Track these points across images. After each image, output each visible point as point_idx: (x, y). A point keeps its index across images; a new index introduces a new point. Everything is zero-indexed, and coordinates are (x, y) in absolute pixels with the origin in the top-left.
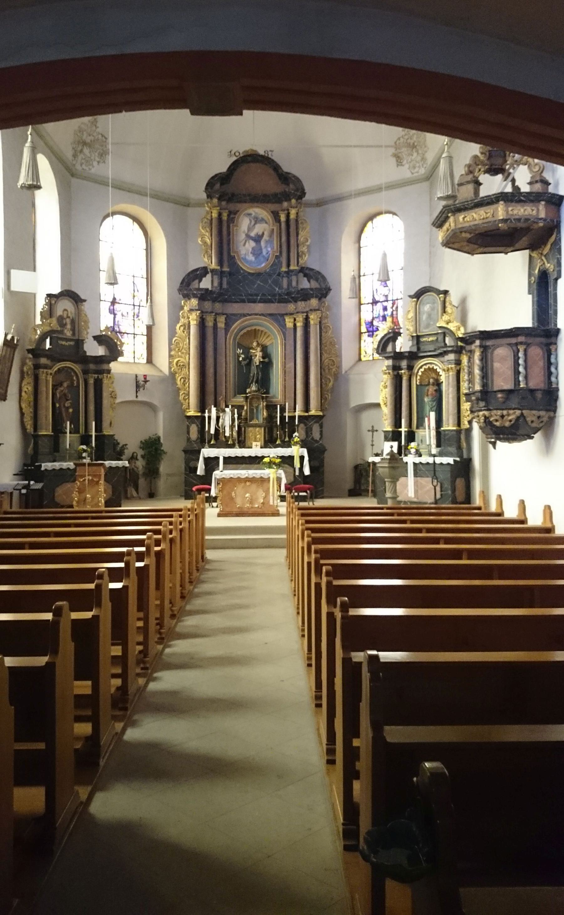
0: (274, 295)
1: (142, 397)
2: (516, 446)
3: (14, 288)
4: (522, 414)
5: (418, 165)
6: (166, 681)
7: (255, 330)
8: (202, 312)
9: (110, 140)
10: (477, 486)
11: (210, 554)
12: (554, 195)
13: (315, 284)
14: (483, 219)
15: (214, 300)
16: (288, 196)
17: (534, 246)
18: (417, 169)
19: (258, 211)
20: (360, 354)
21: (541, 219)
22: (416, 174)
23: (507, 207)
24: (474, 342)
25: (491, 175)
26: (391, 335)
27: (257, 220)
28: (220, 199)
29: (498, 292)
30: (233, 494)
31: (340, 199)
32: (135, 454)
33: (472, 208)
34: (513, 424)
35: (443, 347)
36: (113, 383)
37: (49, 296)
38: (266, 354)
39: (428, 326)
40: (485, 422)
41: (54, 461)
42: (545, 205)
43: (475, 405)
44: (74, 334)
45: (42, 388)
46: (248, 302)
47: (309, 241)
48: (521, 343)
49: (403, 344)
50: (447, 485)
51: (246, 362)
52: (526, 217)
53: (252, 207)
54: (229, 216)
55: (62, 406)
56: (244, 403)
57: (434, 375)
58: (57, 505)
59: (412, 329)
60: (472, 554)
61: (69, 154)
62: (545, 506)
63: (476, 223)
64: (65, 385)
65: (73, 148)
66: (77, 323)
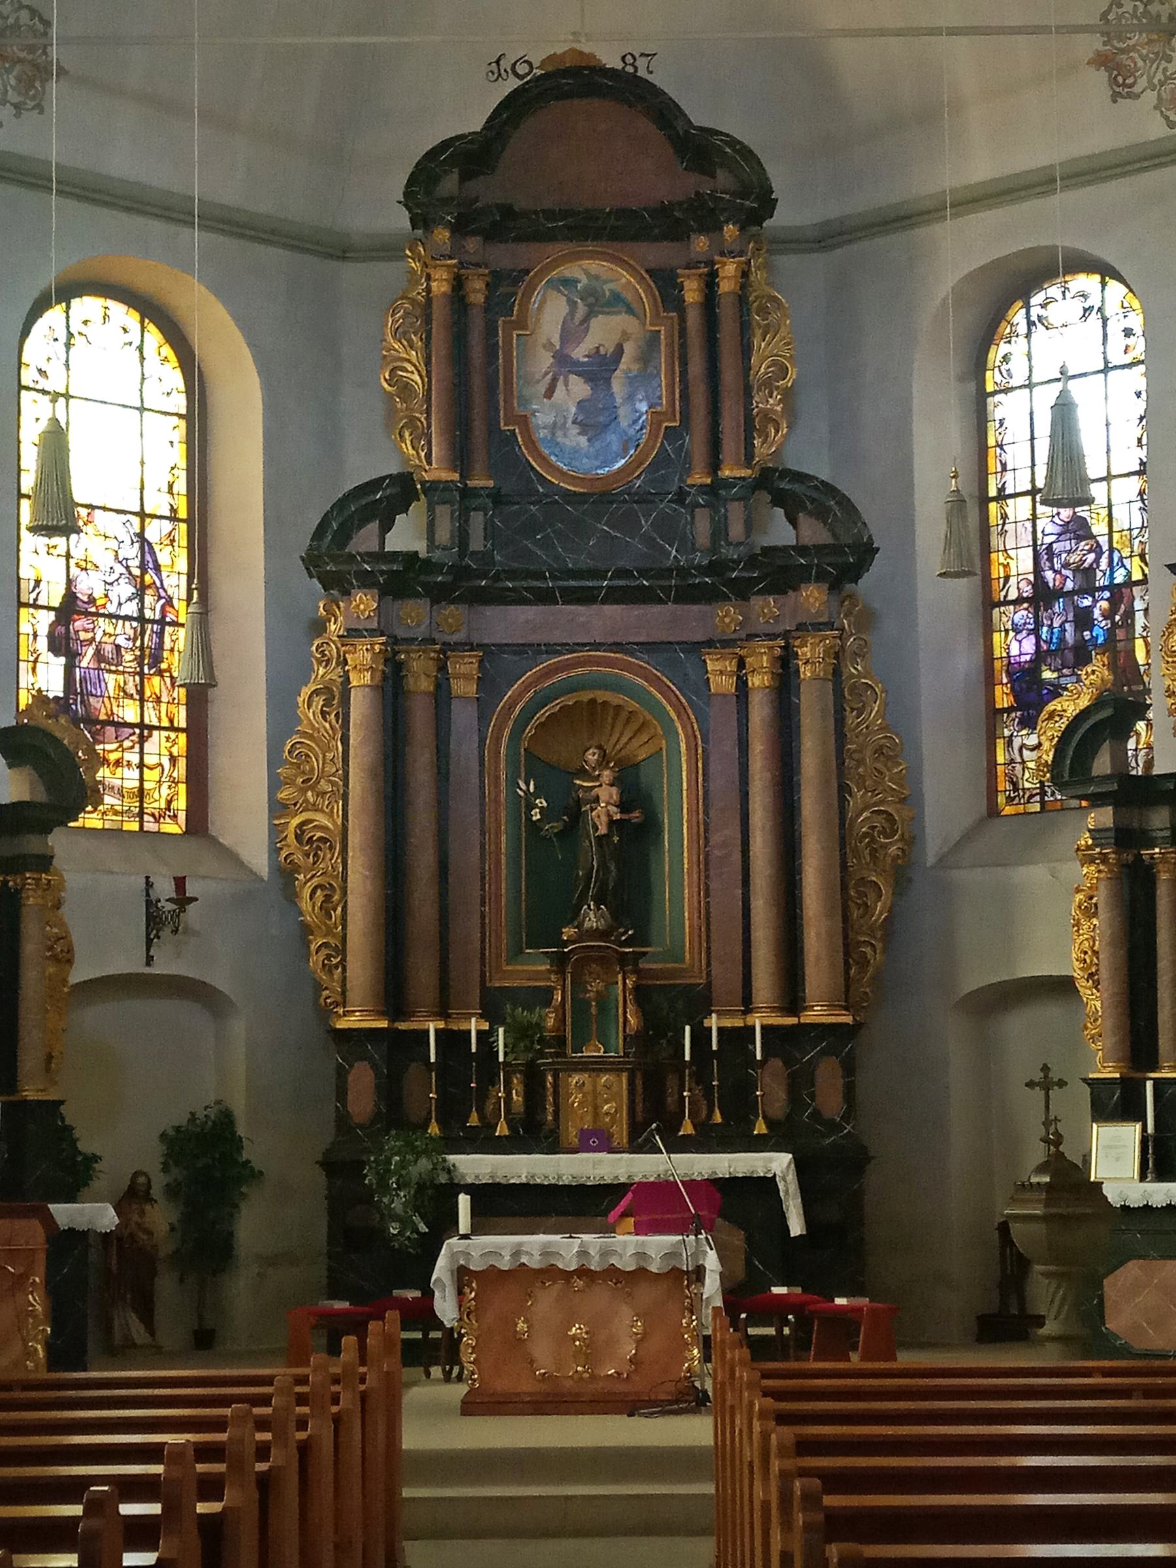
0: (666, 573)
7: (593, 701)
8: (395, 640)
13: (813, 532)
15: (439, 595)
19: (592, 269)
20: (992, 791)
26: (1107, 713)
27: (599, 302)
28: (460, 229)
30: (521, 1326)
31: (902, 219)
32: (142, 1180)
36: (58, 905)
47: (792, 374)
51: (557, 826)
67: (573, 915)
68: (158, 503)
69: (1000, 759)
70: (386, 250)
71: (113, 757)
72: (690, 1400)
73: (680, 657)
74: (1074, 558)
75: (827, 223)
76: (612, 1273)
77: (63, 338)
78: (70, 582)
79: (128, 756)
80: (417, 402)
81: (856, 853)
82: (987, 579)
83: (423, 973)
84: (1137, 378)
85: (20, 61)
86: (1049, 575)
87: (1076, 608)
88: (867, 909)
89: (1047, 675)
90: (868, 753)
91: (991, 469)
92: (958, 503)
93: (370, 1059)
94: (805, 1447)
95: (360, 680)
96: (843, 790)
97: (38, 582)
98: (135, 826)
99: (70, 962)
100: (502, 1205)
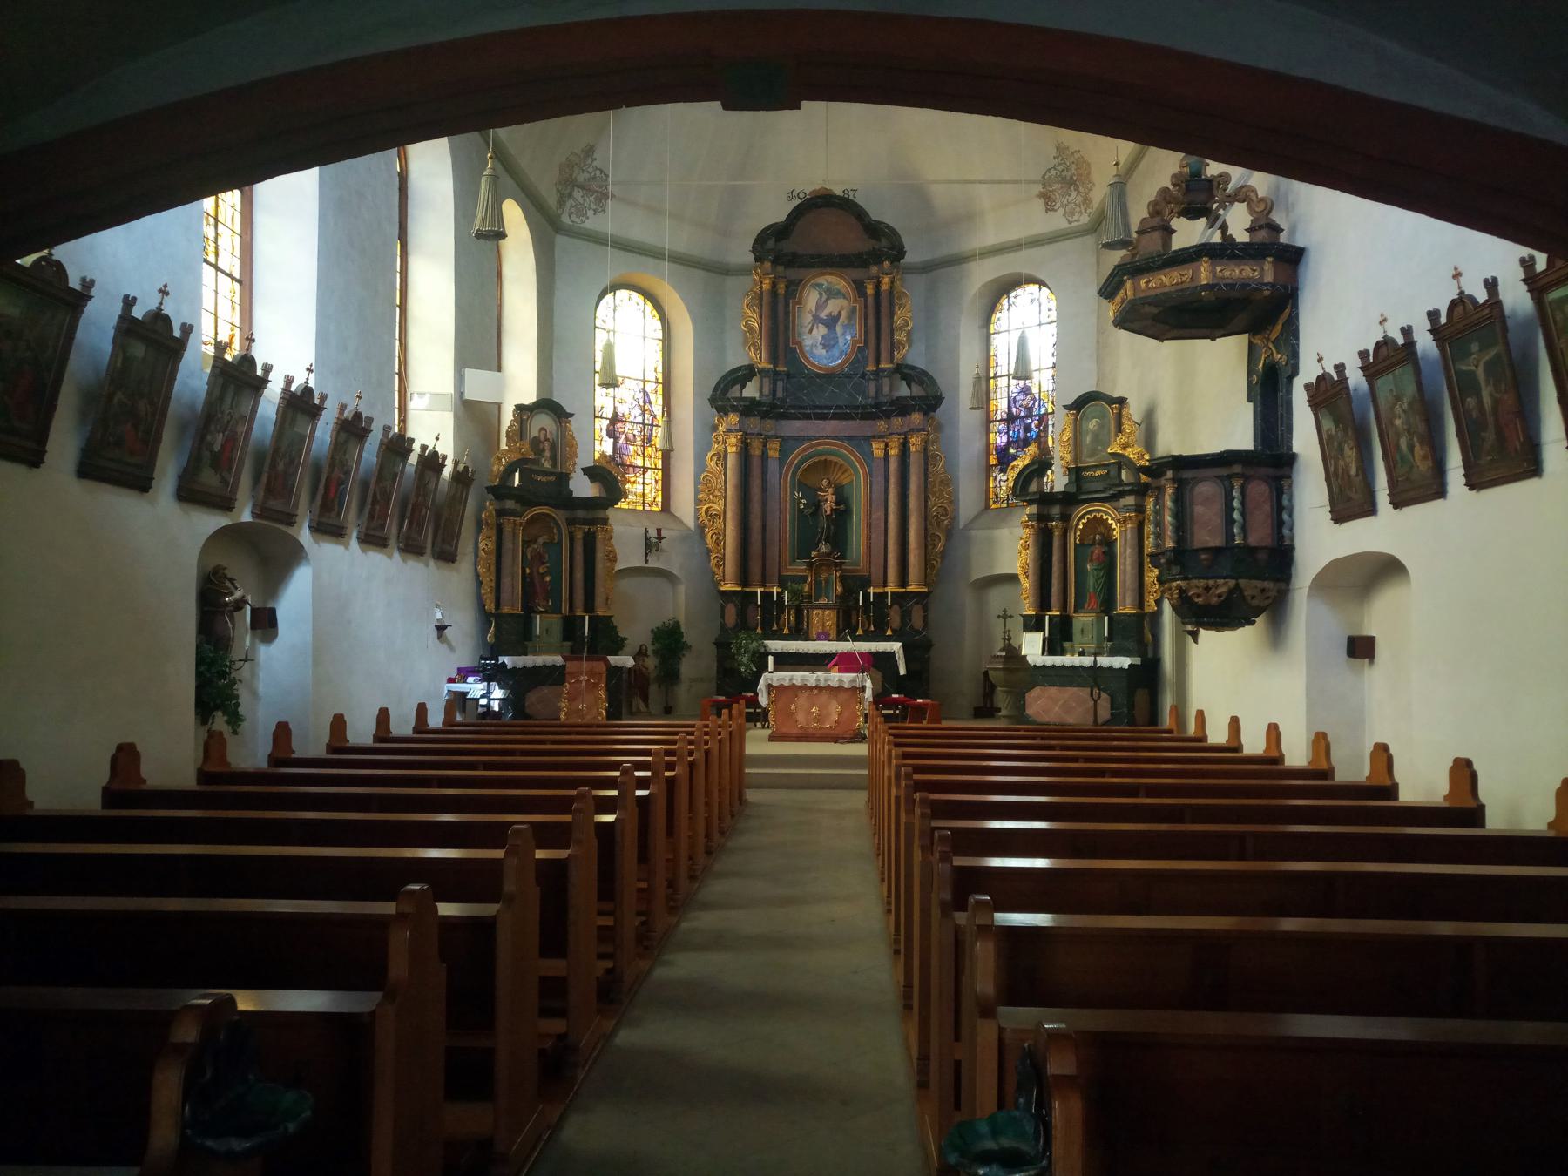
0: (857, 407)
1: (654, 563)
2: (1228, 635)
10: (1168, 701)
11: (751, 795)
13: (917, 391)
15: (764, 416)
17: (1255, 327)
19: (831, 280)
20: (987, 499)
23: (1213, 266)
27: (831, 294)
28: (775, 262)
31: (958, 260)
33: (1160, 268)
37: (520, 408)
38: (842, 499)
39: (1093, 453)
40: (1180, 597)
44: (554, 465)
45: (508, 544)
48: (1236, 475)
53: (823, 274)
54: (787, 287)
59: (1068, 457)
60: (1152, 791)
64: (541, 540)
66: (561, 447)
67: (816, 547)
68: (651, 376)
70: (743, 271)
72: (859, 738)
73: (861, 443)
76: (829, 688)
80: (756, 335)
83: (755, 569)
88: (935, 546)
92: (978, 378)
94: (906, 756)
96: (926, 498)
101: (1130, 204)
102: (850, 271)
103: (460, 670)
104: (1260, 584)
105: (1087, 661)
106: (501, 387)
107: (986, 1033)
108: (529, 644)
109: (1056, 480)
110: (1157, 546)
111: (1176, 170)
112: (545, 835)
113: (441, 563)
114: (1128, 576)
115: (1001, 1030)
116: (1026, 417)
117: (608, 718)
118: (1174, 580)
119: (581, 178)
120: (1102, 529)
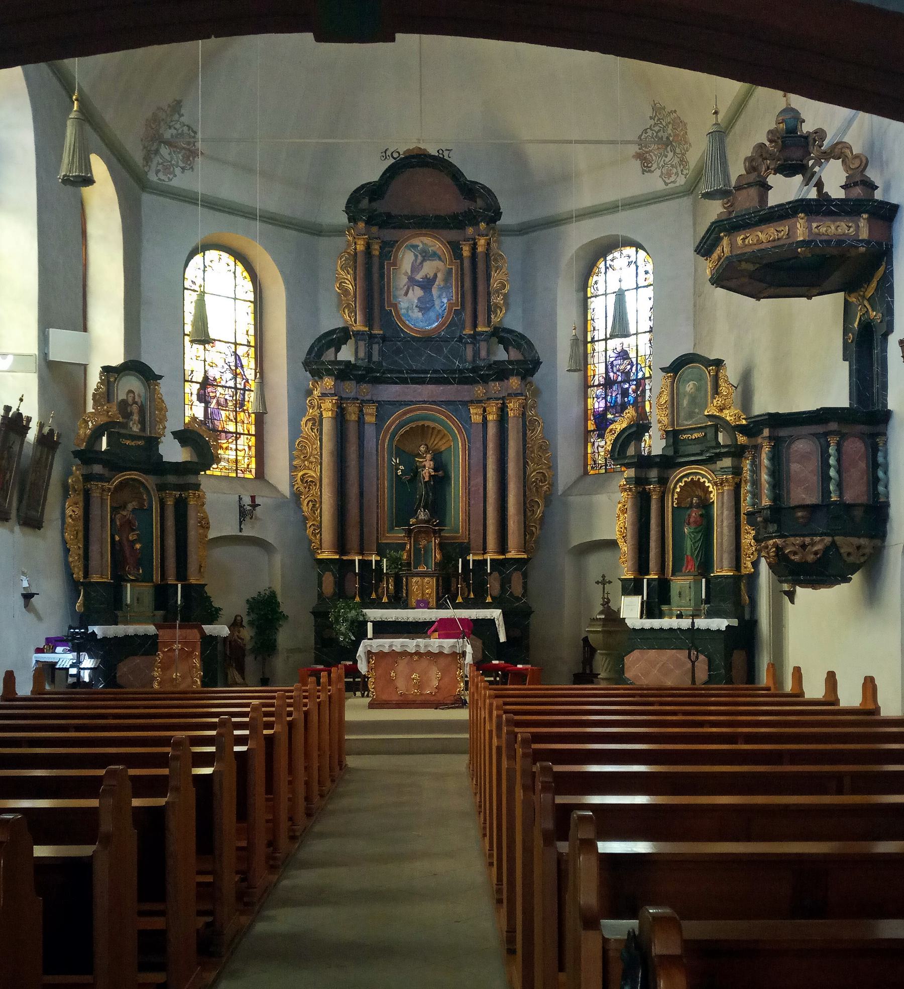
1: (247, 532)
3: (52, 358)
4: (833, 543)
5: (674, 170)
6: (280, 921)
7: (423, 425)
8: (341, 398)
9: (200, 135)
10: (764, 661)
11: (351, 761)
12: (883, 204)
13: (515, 355)
14: (774, 240)
15: (360, 380)
16: (475, 217)
17: (850, 286)
18: (672, 179)
21: (862, 241)
22: (671, 186)
23: (809, 222)
24: (761, 432)
25: (786, 176)
26: (634, 429)
27: (427, 255)
28: (368, 223)
29: (796, 356)
30: (392, 674)
31: (554, 222)
32: (239, 618)
34: (819, 559)
35: (714, 448)
36: (203, 504)
37: (107, 370)
38: (441, 465)
39: (691, 415)
40: (777, 555)
41: (116, 623)
42: (868, 219)
43: (762, 530)
44: (143, 429)
45: (95, 511)
46: (412, 383)
47: (508, 287)
49: (654, 443)
50: (719, 661)
51: (408, 477)
52: (840, 238)
55: (124, 539)
56: (406, 540)
57: (699, 492)
58: (120, 687)
59: (665, 420)
61: (137, 156)
62: (866, 678)
63: (763, 246)
64: (130, 507)
65: (144, 147)
66: (150, 410)
67: (414, 514)
69: (589, 451)
70: (338, 232)
71: (224, 446)
72: (460, 703)
73: (459, 407)
74: (622, 367)
75: (523, 223)
76: (429, 653)
77: (202, 268)
78: (205, 372)
79: (230, 446)
81: (530, 489)
82: (586, 377)
84: (650, 292)
85: (184, 148)
86: (611, 374)
87: (622, 388)
89: (609, 416)
90: (536, 448)
91: (589, 329)
92: (575, 340)
93: (332, 571)
95: (327, 414)
96: (525, 464)
97: (192, 371)
98: (234, 475)
99: (208, 528)
100: (384, 629)
101: (730, 163)
102: (445, 232)
103: (48, 640)
104: (855, 541)
105: (685, 624)
106: (87, 348)
107: (590, 946)
108: (119, 613)
109: (654, 443)
110: (753, 505)
111: (773, 126)
112: (144, 787)
113: (28, 530)
114: (725, 538)
115: (605, 941)
116: (624, 382)
117: (204, 684)
118: (772, 538)
119: (168, 134)
120: (699, 492)
